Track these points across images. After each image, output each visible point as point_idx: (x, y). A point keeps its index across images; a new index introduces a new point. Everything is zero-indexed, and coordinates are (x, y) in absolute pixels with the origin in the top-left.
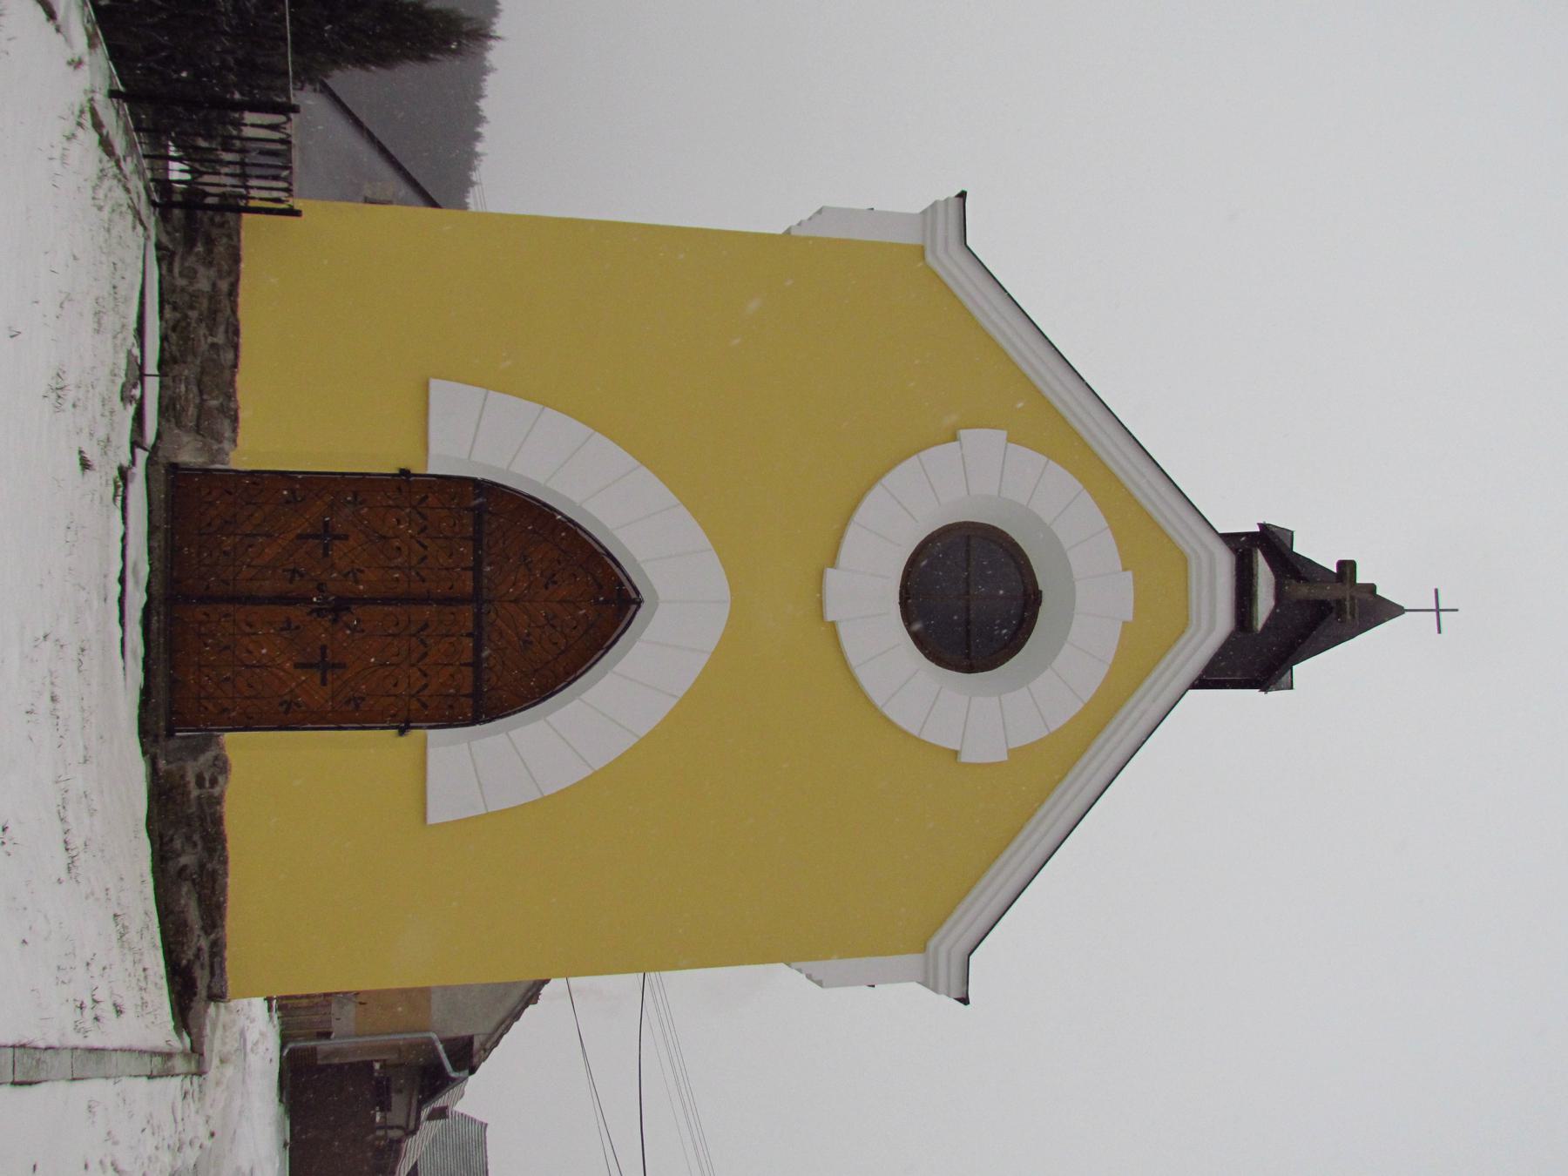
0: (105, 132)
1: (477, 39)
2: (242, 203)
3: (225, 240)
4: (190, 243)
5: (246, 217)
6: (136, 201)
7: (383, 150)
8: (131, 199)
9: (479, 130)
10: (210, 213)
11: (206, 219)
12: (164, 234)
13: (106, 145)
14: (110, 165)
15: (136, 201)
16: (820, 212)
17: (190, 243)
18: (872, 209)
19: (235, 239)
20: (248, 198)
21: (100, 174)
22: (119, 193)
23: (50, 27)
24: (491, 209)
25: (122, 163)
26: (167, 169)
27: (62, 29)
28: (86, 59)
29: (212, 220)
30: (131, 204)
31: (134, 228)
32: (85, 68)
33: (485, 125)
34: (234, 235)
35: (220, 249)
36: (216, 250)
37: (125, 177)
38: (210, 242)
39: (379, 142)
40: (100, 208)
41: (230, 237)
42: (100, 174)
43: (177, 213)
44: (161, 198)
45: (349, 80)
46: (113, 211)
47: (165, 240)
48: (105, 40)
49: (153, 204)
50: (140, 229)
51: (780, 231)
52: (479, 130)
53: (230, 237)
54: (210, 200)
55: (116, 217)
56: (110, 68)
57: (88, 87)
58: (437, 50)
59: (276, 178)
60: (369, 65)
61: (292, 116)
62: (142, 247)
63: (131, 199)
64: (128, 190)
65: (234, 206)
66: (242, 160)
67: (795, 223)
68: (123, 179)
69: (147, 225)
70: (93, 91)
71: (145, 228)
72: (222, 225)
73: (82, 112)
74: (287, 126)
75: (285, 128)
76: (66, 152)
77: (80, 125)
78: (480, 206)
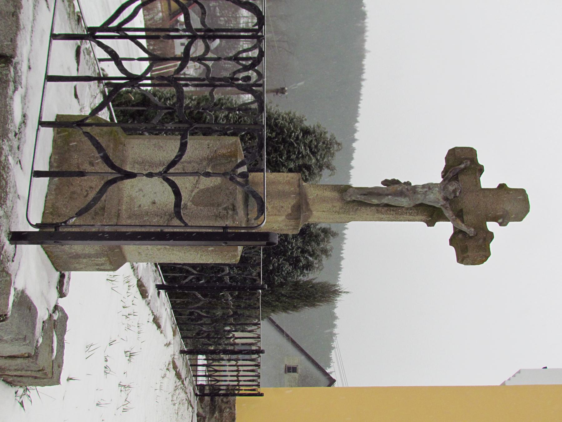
0: (178, 370)
1: (339, 294)
2: (237, 392)
3: (228, 410)
4: (212, 412)
5: (238, 398)
6: (189, 397)
7: (293, 342)
8: (187, 396)
9: (335, 323)
10: (222, 397)
11: (220, 400)
12: (201, 408)
13: (178, 375)
14: (179, 383)
15: (189, 397)
16: (519, 372)
17: (212, 412)
18: (546, 368)
19: (233, 409)
20: (239, 390)
21: (175, 388)
22: (183, 396)
23: (159, 332)
24: (350, 385)
25: (185, 382)
26: (197, 359)
27: (163, 332)
28: (172, 342)
29: (222, 400)
30: (187, 398)
31: (188, 408)
32: (171, 346)
33: (337, 320)
34: (232, 407)
35: (226, 414)
36: (224, 415)
37: (185, 387)
38: (221, 411)
39: (291, 339)
40: (174, 404)
41: (231, 408)
42: (175, 388)
43: (207, 398)
44: (200, 392)
45: (280, 317)
46: (180, 404)
47: (201, 411)
48: (175, 315)
49: (196, 395)
50: (190, 409)
51: (499, 384)
52: (335, 323)
53: (231, 408)
54: (221, 392)
55: (181, 405)
56: (181, 342)
57: (172, 353)
58: (320, 301)
59: (253, 381)
60: (287, 311)
61: (261, 355)
62: (191, 417)
63: (187, 396)
64: (186, 393)
65: (232, 392)
66: (237, 374)
67: (506, 379)
68: (184, 389)
69: (193, 406)
70: (174, 355)
71: (193, 408)
72: (227, 402)
73: (169, 364)
74: (259, 359)
75: (258, 360)
76: (162, 384)
77: (168, 369)
78: (344, 384)
